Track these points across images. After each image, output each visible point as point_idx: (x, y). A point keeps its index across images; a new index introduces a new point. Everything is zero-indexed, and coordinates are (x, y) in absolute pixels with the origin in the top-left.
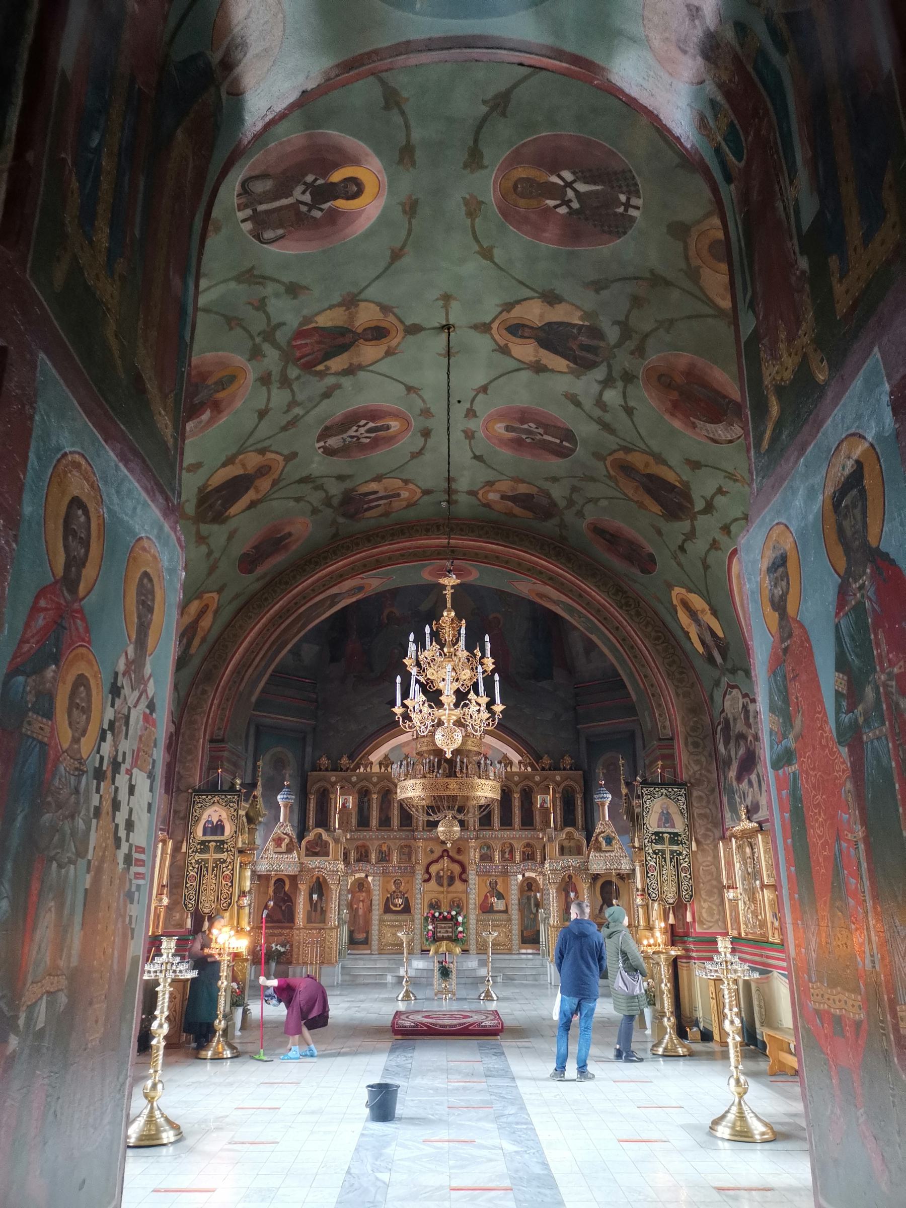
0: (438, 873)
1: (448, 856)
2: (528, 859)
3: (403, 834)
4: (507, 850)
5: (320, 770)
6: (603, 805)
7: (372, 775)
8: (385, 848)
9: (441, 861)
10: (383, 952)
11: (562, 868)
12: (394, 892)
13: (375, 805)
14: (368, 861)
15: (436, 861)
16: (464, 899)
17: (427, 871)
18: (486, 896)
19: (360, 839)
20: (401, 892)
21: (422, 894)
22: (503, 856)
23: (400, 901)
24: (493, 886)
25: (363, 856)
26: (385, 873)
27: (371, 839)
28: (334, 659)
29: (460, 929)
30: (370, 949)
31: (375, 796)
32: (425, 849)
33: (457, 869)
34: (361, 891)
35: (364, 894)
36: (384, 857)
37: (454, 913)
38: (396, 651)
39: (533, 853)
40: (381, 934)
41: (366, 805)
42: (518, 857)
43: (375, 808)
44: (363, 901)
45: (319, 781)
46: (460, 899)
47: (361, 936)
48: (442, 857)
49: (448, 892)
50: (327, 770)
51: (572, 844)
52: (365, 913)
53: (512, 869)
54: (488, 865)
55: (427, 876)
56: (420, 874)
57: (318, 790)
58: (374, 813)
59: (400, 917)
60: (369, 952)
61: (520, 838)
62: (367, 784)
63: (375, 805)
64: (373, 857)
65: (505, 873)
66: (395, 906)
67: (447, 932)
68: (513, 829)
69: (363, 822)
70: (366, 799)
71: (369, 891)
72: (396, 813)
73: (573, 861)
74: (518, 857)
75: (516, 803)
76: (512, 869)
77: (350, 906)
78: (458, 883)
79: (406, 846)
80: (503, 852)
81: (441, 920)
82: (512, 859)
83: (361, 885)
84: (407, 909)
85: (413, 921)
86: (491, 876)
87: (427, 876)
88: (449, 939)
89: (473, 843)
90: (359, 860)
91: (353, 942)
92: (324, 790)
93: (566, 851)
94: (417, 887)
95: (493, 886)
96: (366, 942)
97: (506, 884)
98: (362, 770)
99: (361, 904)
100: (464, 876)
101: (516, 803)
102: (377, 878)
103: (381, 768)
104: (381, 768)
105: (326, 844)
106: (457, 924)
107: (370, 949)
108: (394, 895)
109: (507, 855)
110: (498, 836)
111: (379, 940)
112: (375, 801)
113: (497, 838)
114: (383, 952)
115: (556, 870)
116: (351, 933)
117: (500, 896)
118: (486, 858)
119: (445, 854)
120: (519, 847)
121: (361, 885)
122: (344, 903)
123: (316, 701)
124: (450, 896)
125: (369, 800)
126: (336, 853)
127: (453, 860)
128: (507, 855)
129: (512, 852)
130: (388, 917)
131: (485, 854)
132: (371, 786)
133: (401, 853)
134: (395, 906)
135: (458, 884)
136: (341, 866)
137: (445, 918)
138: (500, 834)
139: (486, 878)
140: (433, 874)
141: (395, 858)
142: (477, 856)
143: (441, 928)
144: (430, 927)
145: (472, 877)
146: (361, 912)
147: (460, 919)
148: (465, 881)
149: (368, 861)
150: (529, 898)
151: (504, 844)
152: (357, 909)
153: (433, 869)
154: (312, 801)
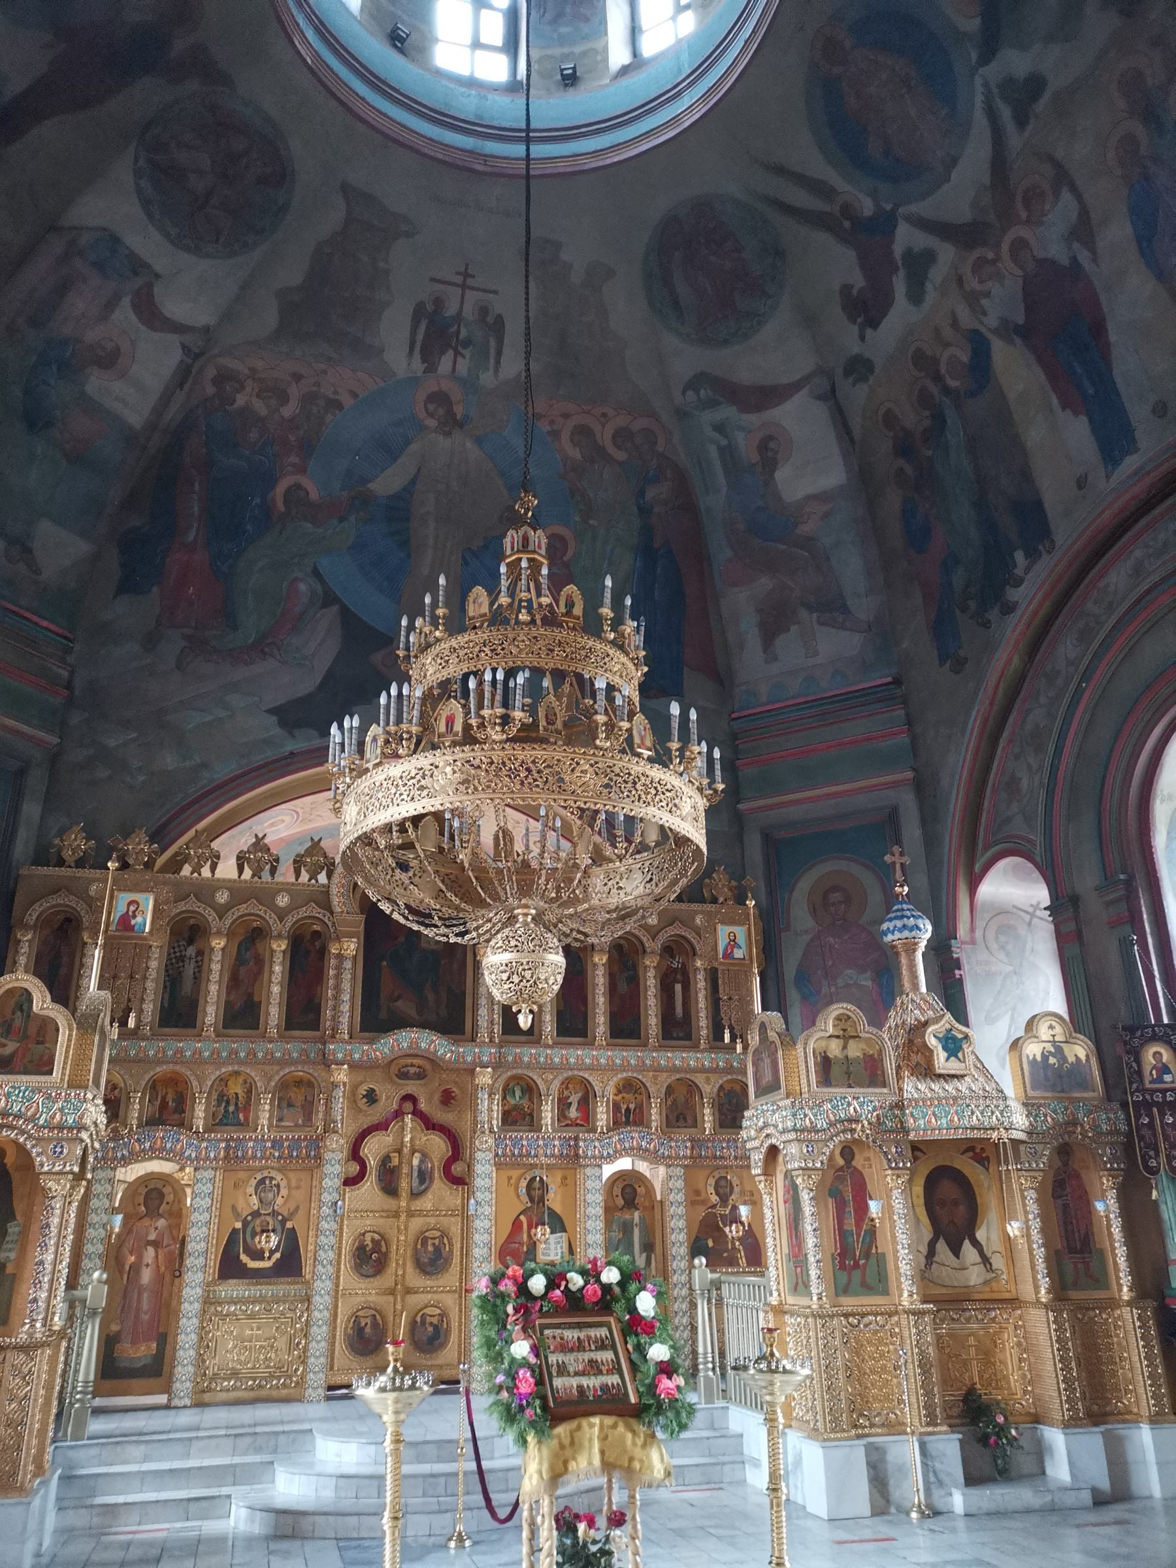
0: (386, 1159)
1: (416, 1113)
2: (627, 1123)
3: (294, 1049)
4: (574, 1099)
5: (61, 862)
6: (911, 948)
7: (216, 885)
8: (236, 1088)
9: (394, 1126)
10: (207, 1397)
11: (832, 1124)
12: (256, 1214)
13: (216, 967)
14: (184, 1124)
15: (382, 1126)
16: (455, 1230)
17: (355, 1154)
18: (517, 1224)
19: (160, 1062)
20: (274, 1214)
21: (336, 1214)
22: (562, 1115)
23: (274, 1239)
24: (536, 1192)
25: (170, 1108)
26: (232, 1161)
27: (198, 1061)
28: (128, 585)
29: (659, 1352)
30: (167, 1389)
31: (218, 943)
32: (353, 1093)
33: (438, 1145)
34: (153, 1212)
35: (161, 1223)
36: (231, 1113)
37: (611, 1276)
38: (302, 587)
39: (640, 1107)
40: (204, 1343)
41: (190, 969)
42: (602, 1117)
43: (215, 976)
44: (156, 1244)
45: (55, 891)
46: (444, 1234)
47: (141, 1352)
48: (398, 1114)
49: (411, 1214)
50: (80, 863)
51: (855, 1050)
52: (159, 1278)
53: (589, 1146)
54: (526, 1137)
55: (354, 1168)
56: (335, 1165)
57: (43, 923)
58: (213, 988)
59: (267, 1290)
60: (162, 1399)
61: (611, 1068)
62: (200, 908)
63: (216, 967)
64: (200, 1115)
65: (572, 1160)
66: (258, 1255)
67: (594, 1368)
68: (591, 1044)
69: (179, 1013)
70: (191, 951)
71: (178, 1215)
72: (276, 989)
73: (862, 1104)
74: (602, 1117)
75: (599, 980)
76: (589, 1146)
77: (114, 1260)
78: (439, 1185)
79: (299, 1083)
80: (563, 1104)
81: (558, 1310)
82: (587, 1118)
83: (154, 1197)
84: (290, 1264)
85: (308, 1299)
86: (533, 1166)
87: (354, 1168)
88: (610, 1404)
89: (485, 1077)
90: (152, 1122)
91: (112, 1372)
92: (68, 920)
93: (836, 1071)
94: (327, 1198)
95: (536, 1192)
96: (156, 1371)
97: (570, 1185)
98: (186, 870)
99: (151, 1251)
100: (458, 1169)
101: (599, 980)
102: (209, 1174)
103: (241, 870)
104: (241, 870)
105: (47, 1029)
106: (636, 1325)
107: (167, 1389)
108: (253, 1224)
109: (573, 1113)
110: (557, 1058)
111: (200, 1361)
112: (217, 956)
113: (550, 1067)
114: (207, 1397)
115: (814, 1129)
116: (109, 1344)
117: (558, 1224)
118: (519, 1117)
119: (408, 1106)
120: (606, 1089)
121: (154, 1197)
122: (94, 1248)
123: (69, 686)
124: (416, 1224)
125: (200, 953)
126: (80, 1062)
127: (429, 1124)
128: (573, 1113)
129: (586, 1104)
130: (233, 1288)
131: (516, 1107)
132: (211, 915)
133: (283, 1102)
134: (258, 1255)
135: (440, 1192)
136: (95, 1113)
137: (574, 1302)
138: (557, 1056)
139: (515, 1174)
140: (372, 1163)
141: (264, 1114)
142: (497, 1114)
143: (564, 1348)
144: (521, 1349)
145: (484, 1171)
146: (146, 1276)
147: (646, 1303)
148: (460, 1181)
149: (184, 1124)
150: (627, 1228)
151: (566, 1083)
152: (135, 1269)
153: (372, 1150)
154: (24, 949)
